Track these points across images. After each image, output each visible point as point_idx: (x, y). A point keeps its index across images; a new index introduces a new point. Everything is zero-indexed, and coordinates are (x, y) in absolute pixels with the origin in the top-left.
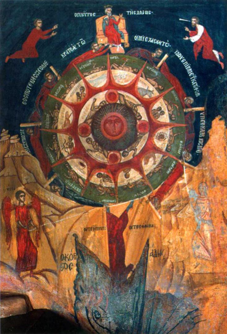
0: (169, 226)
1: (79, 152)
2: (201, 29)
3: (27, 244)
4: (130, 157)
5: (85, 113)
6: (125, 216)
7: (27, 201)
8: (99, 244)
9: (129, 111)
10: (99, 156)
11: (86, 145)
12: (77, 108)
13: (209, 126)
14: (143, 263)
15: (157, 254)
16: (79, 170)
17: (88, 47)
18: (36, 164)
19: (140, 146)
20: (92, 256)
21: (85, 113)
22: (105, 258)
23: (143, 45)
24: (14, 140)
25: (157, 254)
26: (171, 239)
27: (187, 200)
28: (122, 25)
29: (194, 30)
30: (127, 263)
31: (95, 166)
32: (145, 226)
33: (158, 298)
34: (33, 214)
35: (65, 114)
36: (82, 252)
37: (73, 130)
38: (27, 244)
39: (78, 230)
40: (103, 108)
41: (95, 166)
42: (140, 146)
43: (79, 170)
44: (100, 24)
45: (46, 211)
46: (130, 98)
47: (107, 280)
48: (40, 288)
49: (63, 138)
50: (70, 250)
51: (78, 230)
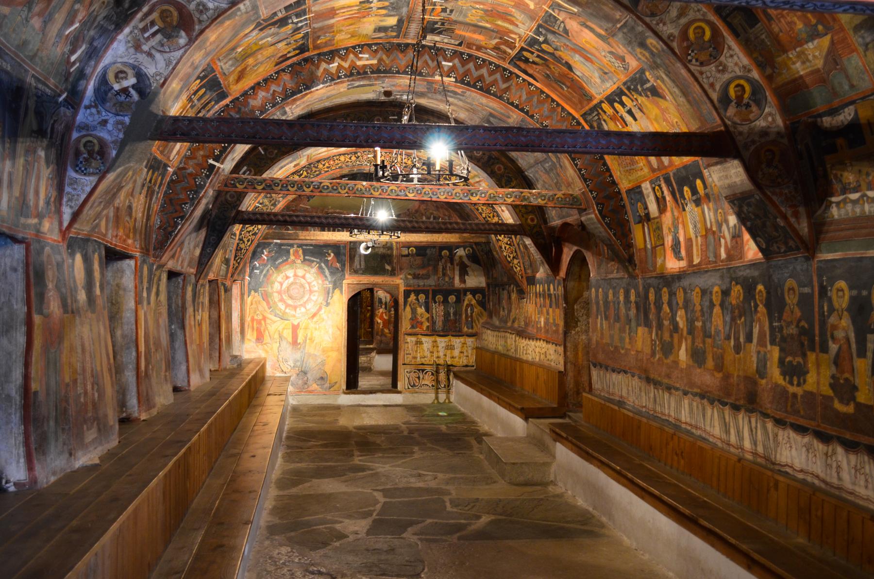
0: (316, 329)
1: (282, 300)
2: (332, 255)
3: (628, 410)
4: (302, 302)
5: (285, 286)
6: (298, 324)
7: (260, 317)
8: (288, 334)
9: (302, 286)
10: (290, 302)
11: (285, 298)
12: (281, 284)
13: (333, 292)
14: (305, 341)
15: (311, 339)
16: (281, 306)
17: (287, 260)
18: (264, 304)
19: (305, 299)
20: (286, 339)
21: (285, 286)
22: (290, 340)
23: (309, 260)
24: (256, 294)
25: (311, 339)
26: (316, 334)
27: (323, 320)
28: (301, 252)
29: (329, 255)
30: (299, 341)
31: (287, 306)
32: (306, 328)
33: (310, 355)
34: (263, 322)
35: (277, 286)
36: (281, 337)
37: (279, 293)
38: (628, 410)
39: (280, 328)
40: (292, 284)
41: (287, 306)
42: (305, 299)
43: (281, 306)
44: (291, 251)
45: (268, 321)
46: (303, 281)
47: (50, 169)
48: (420, 159)
49: (275, 295)
50: (276, 336)
51: (280, 328)
